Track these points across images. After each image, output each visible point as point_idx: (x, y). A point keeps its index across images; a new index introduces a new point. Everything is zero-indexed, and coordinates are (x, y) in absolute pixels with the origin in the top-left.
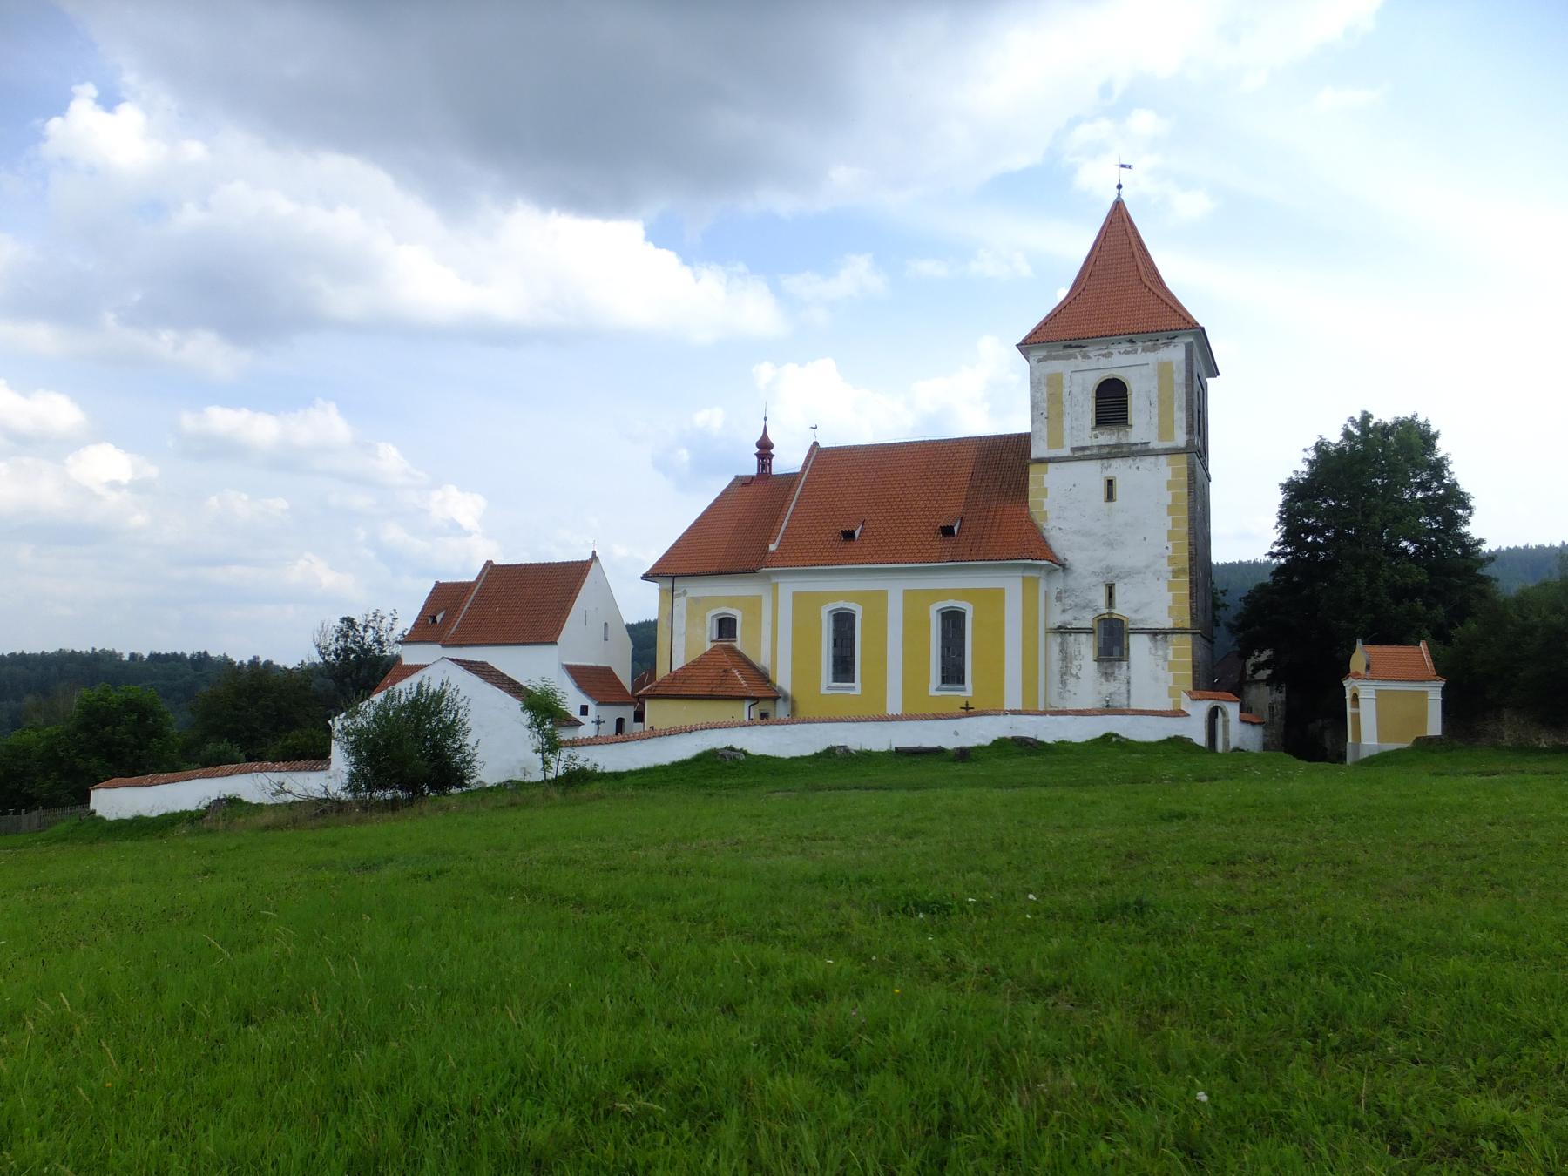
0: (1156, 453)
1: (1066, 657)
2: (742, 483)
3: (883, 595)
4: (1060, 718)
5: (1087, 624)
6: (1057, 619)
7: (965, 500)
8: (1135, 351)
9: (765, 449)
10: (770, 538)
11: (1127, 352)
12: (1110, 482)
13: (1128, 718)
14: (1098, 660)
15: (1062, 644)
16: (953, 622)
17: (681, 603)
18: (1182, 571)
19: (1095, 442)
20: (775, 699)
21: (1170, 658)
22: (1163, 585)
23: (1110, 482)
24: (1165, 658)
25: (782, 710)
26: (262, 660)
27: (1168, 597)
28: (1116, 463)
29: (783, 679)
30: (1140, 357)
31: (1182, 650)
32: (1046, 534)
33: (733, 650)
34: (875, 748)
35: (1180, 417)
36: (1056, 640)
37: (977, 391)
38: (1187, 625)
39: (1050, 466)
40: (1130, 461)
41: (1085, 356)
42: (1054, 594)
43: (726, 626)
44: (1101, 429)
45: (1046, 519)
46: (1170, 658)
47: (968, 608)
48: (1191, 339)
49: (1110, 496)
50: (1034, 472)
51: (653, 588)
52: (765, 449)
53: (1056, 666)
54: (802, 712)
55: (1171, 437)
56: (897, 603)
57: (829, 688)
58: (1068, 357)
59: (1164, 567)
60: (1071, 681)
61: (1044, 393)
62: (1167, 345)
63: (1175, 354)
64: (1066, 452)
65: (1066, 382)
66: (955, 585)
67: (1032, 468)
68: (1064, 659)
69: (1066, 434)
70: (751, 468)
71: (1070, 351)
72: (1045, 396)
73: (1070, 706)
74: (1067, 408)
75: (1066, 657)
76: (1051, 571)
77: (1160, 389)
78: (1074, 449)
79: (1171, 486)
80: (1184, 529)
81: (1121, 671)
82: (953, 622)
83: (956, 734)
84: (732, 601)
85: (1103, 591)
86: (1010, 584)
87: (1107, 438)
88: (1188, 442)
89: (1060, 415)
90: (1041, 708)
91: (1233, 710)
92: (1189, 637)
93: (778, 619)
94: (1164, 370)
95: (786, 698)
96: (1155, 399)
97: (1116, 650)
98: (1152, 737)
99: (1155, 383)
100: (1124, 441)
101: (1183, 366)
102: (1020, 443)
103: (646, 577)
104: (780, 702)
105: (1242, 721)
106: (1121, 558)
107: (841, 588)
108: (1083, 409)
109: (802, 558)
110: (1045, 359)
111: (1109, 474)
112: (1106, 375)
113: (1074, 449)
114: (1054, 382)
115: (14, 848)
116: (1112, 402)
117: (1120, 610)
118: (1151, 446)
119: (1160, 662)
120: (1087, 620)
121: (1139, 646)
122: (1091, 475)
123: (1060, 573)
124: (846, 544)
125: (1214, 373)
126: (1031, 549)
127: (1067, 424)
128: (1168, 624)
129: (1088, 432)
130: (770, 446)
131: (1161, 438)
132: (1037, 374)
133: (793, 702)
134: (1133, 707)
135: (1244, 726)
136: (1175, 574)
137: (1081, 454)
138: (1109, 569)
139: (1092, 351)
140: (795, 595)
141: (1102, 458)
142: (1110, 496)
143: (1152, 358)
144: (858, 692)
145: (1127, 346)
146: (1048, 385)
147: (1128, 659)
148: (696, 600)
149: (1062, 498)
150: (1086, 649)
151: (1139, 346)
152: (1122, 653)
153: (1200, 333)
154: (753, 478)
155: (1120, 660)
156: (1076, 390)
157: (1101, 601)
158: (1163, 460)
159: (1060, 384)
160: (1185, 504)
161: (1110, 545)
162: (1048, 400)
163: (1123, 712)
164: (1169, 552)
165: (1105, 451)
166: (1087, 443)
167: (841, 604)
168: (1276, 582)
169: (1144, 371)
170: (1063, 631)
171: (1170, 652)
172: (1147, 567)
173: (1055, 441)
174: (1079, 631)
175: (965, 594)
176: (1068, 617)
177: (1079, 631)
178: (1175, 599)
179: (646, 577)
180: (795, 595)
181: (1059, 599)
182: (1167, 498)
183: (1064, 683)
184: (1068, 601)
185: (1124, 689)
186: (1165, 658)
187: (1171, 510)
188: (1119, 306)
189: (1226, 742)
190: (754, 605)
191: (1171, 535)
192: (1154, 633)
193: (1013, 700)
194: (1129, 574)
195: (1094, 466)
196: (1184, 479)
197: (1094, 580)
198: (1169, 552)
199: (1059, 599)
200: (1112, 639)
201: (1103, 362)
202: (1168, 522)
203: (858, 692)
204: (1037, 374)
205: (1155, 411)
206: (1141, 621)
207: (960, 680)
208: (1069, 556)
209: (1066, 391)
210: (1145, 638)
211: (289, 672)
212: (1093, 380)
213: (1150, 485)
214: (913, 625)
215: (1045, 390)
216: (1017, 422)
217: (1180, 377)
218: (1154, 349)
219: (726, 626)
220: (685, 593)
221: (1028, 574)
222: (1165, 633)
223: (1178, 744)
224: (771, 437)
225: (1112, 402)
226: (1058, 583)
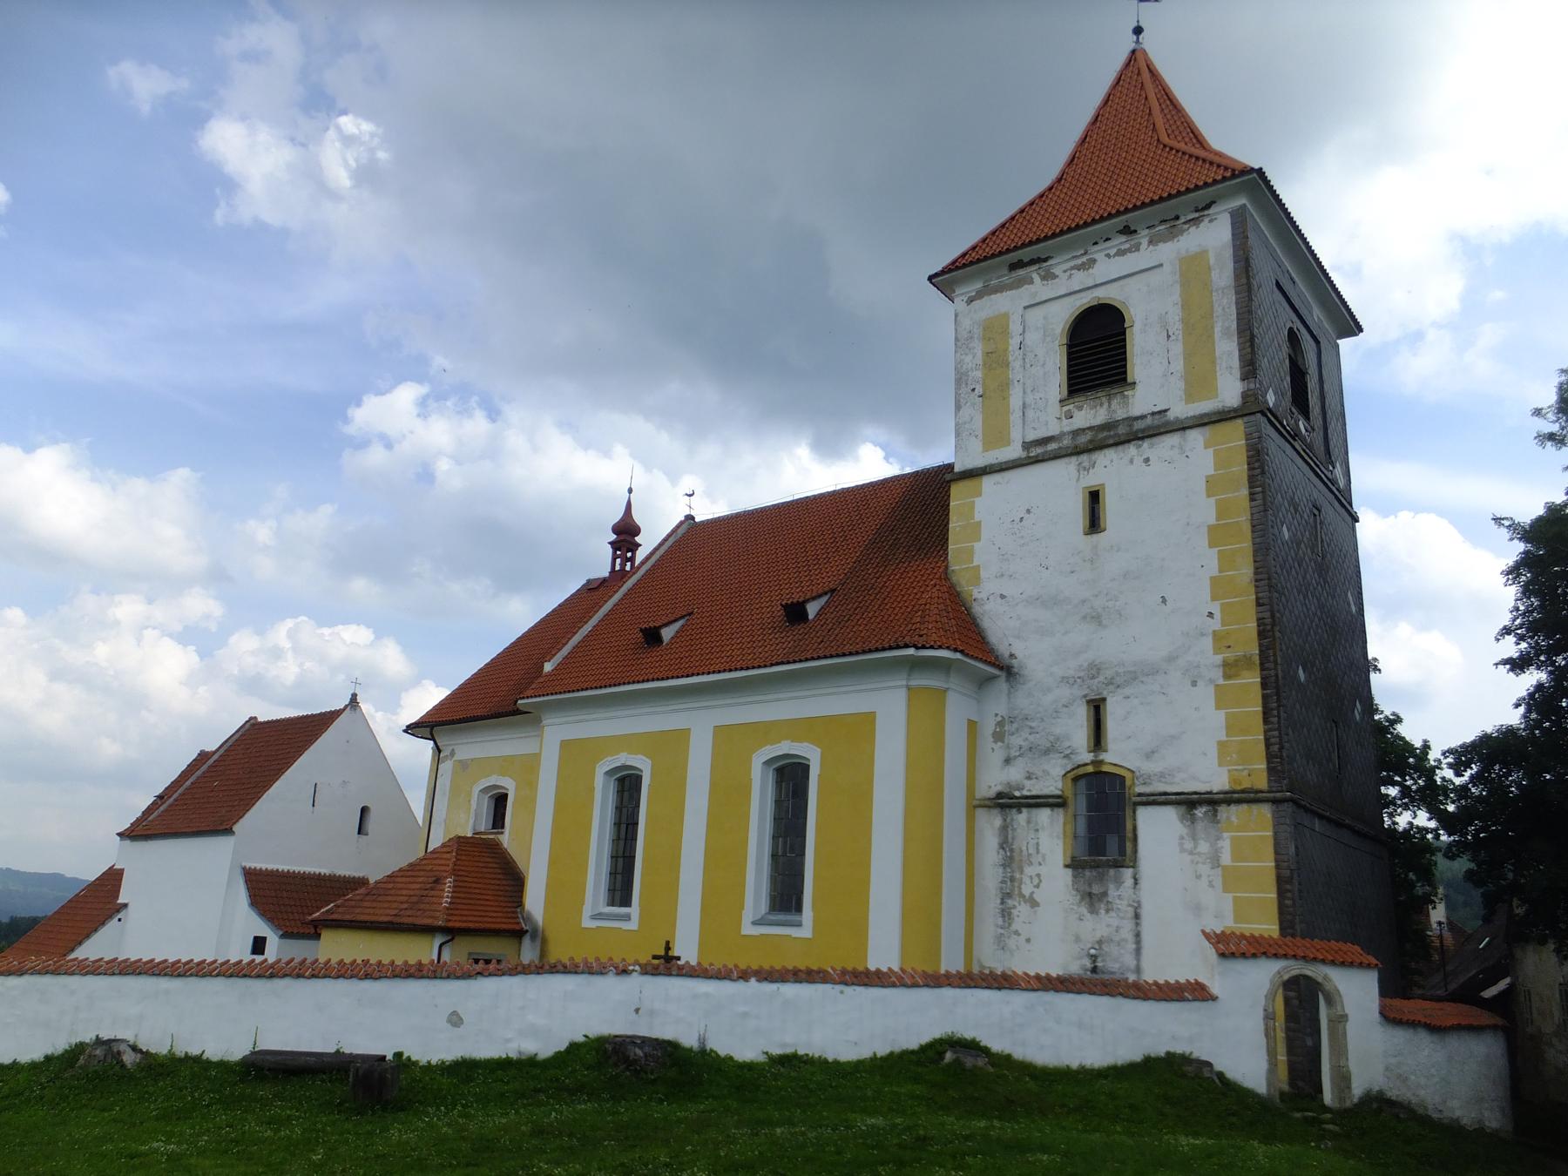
0: (1182, 427)
1: (1011, 859)
2: (594, 591)
3: (683, 736)
4: (790, 990)
6: (994, 779)
8: (1137, 248)
10: (548, 655)
11: (1121, 253)
12: (1094, 497)
13: (1018, 999)
14: (1075, 865)
15: (1004, 829)
16: (791, 779)
17: (446, 767)
18: (1245, 661)
20: (519, 934)
21: (1226, 859)
22: (1206, 694)
23: (1094, 497)
24: (1215, 860)
25: (528, 953)
27: (1216, 719)
29: (535, 901)
30: (1146, 255)
31: (1252, 836)
32: (977, 609)
34: (25, 1058)
36: (990, 824)
38: (1262, 782)
39: (988, 482)
40: (1131, 450)
41: (1049, 276)
42: (989, 727)
44: (1079, 399)
45: (977, 580)
46: (1226, 859)
47: (812, 754)
48: (1241, 201)
49: (1094, 523)
54: (557, 953)
55: (1212, 391)
57: (595, 917)
59: (1207, 657)
60: (1021, 911)
62: (1195, 222)
63: (1212, 236)
64: (1014, 451)
65: (1015, 327)
66: (791, 711)
69: (1015, 417)
71: (1021, 272)
72: (979, 359)
74: (1016, 371)
75: (1011, 859)
76: (984, 682)
78: (1027, 446)
79: (1212, 485)
80: (1245, 571)
81: (1120, 892)
82: (791, 779)
83: (455, 1020)
84: (505, 764)
85: (1082, 714)
86: (884, 704)
87: (1090, 414)
88: (1245, 395)
89: (1004, 387)
90: (951, 961)
91: (1356, 992)
92: (1265, 812)
96: (1176, 327)
97: (1112, 842)
98: (1094, 1055)
99: (1176, 297)
100: (1120, 414)
101: (1228, 253)
104: (526, 941)
105: (1390, 1018)
106: (1115, 646)
110: (980, 295)
111: (1092, 480)
113: (1027, 446)
114: (995, 330)
115: (1433, 1029)
116: (1097, 351)
117: (1117, 755)
118: (1171, 415)
119: (1205, 869)
120: (1051, 780)
121: (1157, 831)
122: (1061, 485)
123: (1002, 685)
125: (1352, 327)
126: (959, 640)
127: (1015, 401)
128: (1216, 780)
129: (1054, 409)
130: (636, 531)
131: (1190, 397)
132: (966, 323)
133: (544, 942)
134: (1149, 976)
135: (1400, 1036)
136: (1231, 668)
137: (1040, 453)
138: (1094, 669)
139: (1059, 265)
140: (565, 745)
141: (1077, 452)
142: (1094, 523)
143: (1168, 252)
145: (1120, 241)
146: (986, 338)
147: (1134, 864)
148: (464, 765)
149: (1009, 548)
150: (1049, 839)
151: (1143, 236)
152: (1122, 852)
153: (1256, 183)
154: (604, 580)
155: (1118, 865)
156: (1032, 338)
157: (1080, 737)
158: (1196, 437)
159: (1005, 333)
160: (1243, 519)
161: (1096, 619)
162: (988, 382)
163: (1004, 982)
164: (1216, 624)
165: (1083, 439)
166: (1053, 429)
167: (624, 758)
168: (1531, 725)
169: (1162, 283)
170: (1006, 802)
171: (1226, 845)
172: (1171, 659)
174: (1036, 802)
176: (1015, 774)
177: (1036, 802)
180: (565, 745)
181: (998, 736)
182: (1206, 511)
183: (1006, 914)
184: (1016, 741)
185: (1127, 933)
186: (1215, 860)
187: (1216, 535)
189: (1342, 1079)
190: (528, 768)
192: (1189, 803)
194: (1135, 675)
196: (1240, 468)
197: (1065, 693)
198: (1216, 624)
199: (998, 736)
200: (1104, 816)
201: (1080, 279)
202: (1210, 561)
203: (633, 925)
204: (966, 323)
205: (1177, 348)
206: (1161, 776)
207: (626, 901)
208: (1019, 648)
209: (1014, 342)
210: (1170, 814)
212: (1061, 315)
213: (1180, 498)
214: (728, 795)
215: (979, 348)
217: (1223, 275)
218: (1173, 234)
220: (453, 753)
221: (920, 681)
222: (1212, 802)
223: (1176, 1084)
224: (637, 517)
225: (1097, 351)
226: (998, 703)
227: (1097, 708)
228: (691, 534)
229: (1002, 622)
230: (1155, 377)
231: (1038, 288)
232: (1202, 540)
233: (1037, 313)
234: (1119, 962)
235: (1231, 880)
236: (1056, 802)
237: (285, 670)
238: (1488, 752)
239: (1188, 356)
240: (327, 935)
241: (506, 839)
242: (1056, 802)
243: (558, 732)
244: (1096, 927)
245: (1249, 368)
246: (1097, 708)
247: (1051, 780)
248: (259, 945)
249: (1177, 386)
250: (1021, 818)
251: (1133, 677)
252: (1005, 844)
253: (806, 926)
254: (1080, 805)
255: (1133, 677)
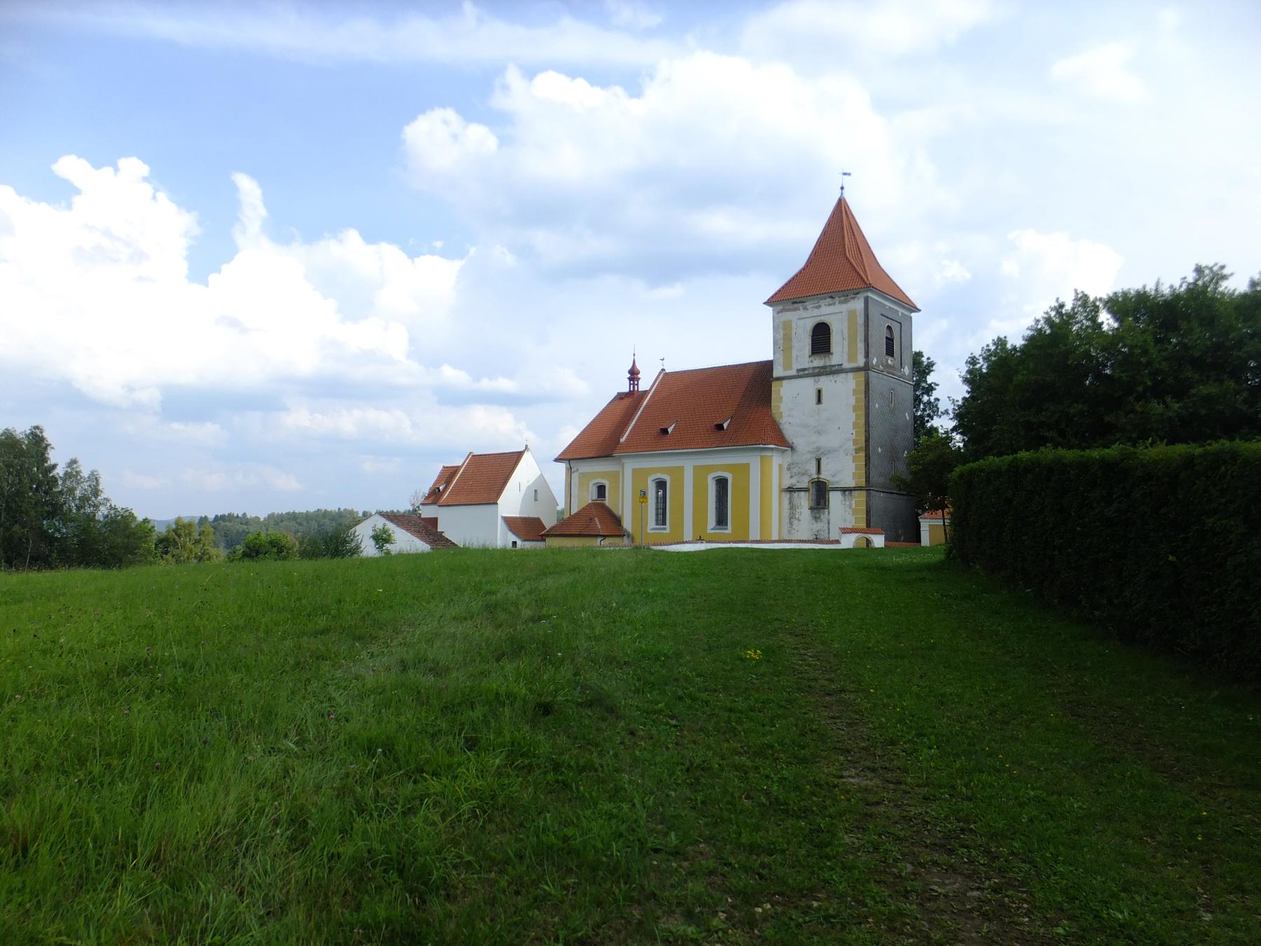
1: (792, 507)
2: (621, 397)
5: (804, 485)
6: (787, 483)
7: (733, 406)
9: (634, 374)
10: (621, 434)
12: (819, 391)
14: (811, 509)
17: (575, 476)
19: (811, 365)
22: (850, 458)
23: (819, 391)
26: (23, 199)
28: (823, 379)
29: (627, 524)
30: (838, 308)
33: (603, 506)
35: (861, 346)
36: (786, 496)
37: (739, 333)
39: (785, 382)
40: (831, 377)
41: (805, 309)
43: (601, 490)
49: (819, 401)
50: (775, 385)
51: (562, 467)
52: (634, 374)
53: (786, 512)
55: (856, 361)
56: (690, 472)
58: (795, 309)
59: (851, 446)
60: (795, 522)
61: (780, 335)
63: (858, 305)
64: (794, 372)
65: (794, 325)
66: (722, 461)
67: (774, 384)
68: (791, 508)
69: (794, 360)
70: (625, 388)
73: (793, 538)
77: (849, 329)
81: (824, 516)
85: (814, 463)
86: (753, 460)
87: (818, 362)
89: (790, 348)
93: (628, 482)
94: (852, 314)
95: (629, 535)
96: (846, 336)
99: (846, 324)
102: (767, 367)
103: (557, 460)
106: (826, 442)
107: (658, 465)
108: (803, 343)
109: (640, 447)
111: (819, 386)
112: (818, 320)
113: (798, 371)
116: (821, 338)
117: (825, 476)
121: (835, 498)
122: (807, 387)
124: (659, 439)
128: (852, 484)
129: (807, 359)
130: (630, 379)
131: (850, 360)
136: (857, 451)
137: (802, 374)
138: (818, 449)
139: (809, 305)
140: (634, 470)
141: (814, 375)
142: (819, 401)
144: (668, 531)
145: (829, 300)
146: (784, 329)
148: (584, 474)
149: (791, 401)
158: (850, 375)
159: (791, 327)
161: (819, 433)
162: (783, 338)
166: (806, 366)
167: (659, 476)
169: (840, 316)
170: (791, 490)
173: (787, 366)
174: (800, 490)
175: (727, 467)
176: (793, 481)
177: (800, 490)
178: (856, 468)
179: (557, 460)
180: (634, 470)
182: (852, 401)
183: (791, 523)
187: (855, 409)
188: (840, 261)
190: (616, 477)
191: (855, 425)
192: (844, 490)
193: (688, 535)
195: (809, 382)
197: (809, 456)
199: (789, 469)
200: (821, 492)
201: (816, 312)
202: (852, 417)
203: (668, 531)
205: (846, 343)
207: (664, 523)
210: (839, 493)
211: (87, 159)
212: (810, 324)
215: (781, 332)
216: (764, 352)
217: (861, 320)
218: (846, 302)
219: (601, 490)
224: (638, 366)
225: (821, 338)
227: (819, 461)
228: (667, 379)
229: (789, 432)
230: (839, 352)
231: (802, 313)
232: (851, 409)
233: (802, 322)
234: (824, 535)
235: (855, 512)
236: (806, 490)
237: (489, 431)
238: (1014, 348)
239: (849, 346)
240: (548, 540)
241: (607, 502)
242: (806, 490)
243: (630, 466)
244: (817, 526)
245: (867, 355)
246: (819, 461)
247: (804, 483)
248: (514, 543)
249: (846, 357)
250: (796, 494)
251: (829, 452)
252: (791, 502)
253: (729, 530)
254: (813, 490)
255: (829, 452)
